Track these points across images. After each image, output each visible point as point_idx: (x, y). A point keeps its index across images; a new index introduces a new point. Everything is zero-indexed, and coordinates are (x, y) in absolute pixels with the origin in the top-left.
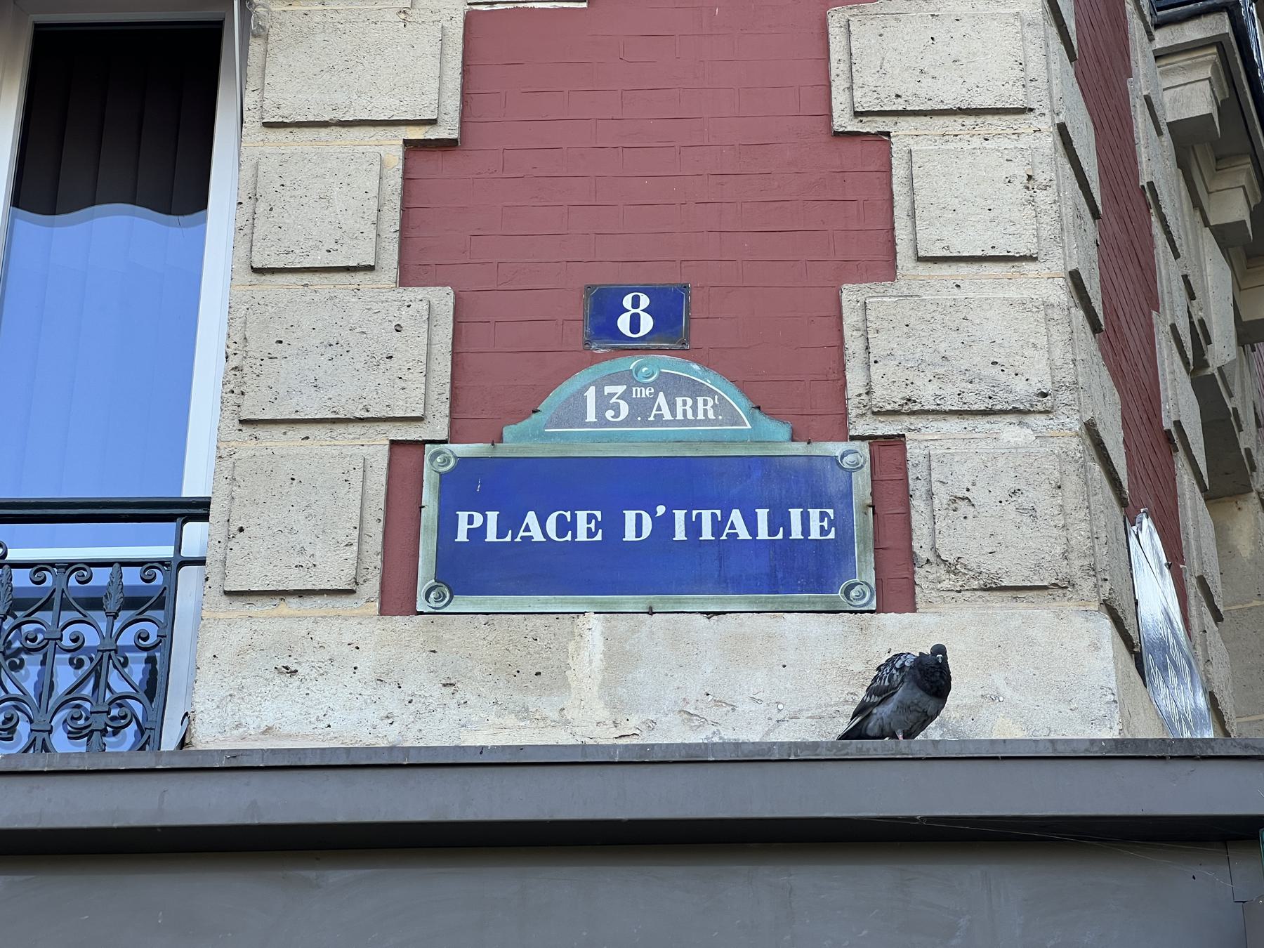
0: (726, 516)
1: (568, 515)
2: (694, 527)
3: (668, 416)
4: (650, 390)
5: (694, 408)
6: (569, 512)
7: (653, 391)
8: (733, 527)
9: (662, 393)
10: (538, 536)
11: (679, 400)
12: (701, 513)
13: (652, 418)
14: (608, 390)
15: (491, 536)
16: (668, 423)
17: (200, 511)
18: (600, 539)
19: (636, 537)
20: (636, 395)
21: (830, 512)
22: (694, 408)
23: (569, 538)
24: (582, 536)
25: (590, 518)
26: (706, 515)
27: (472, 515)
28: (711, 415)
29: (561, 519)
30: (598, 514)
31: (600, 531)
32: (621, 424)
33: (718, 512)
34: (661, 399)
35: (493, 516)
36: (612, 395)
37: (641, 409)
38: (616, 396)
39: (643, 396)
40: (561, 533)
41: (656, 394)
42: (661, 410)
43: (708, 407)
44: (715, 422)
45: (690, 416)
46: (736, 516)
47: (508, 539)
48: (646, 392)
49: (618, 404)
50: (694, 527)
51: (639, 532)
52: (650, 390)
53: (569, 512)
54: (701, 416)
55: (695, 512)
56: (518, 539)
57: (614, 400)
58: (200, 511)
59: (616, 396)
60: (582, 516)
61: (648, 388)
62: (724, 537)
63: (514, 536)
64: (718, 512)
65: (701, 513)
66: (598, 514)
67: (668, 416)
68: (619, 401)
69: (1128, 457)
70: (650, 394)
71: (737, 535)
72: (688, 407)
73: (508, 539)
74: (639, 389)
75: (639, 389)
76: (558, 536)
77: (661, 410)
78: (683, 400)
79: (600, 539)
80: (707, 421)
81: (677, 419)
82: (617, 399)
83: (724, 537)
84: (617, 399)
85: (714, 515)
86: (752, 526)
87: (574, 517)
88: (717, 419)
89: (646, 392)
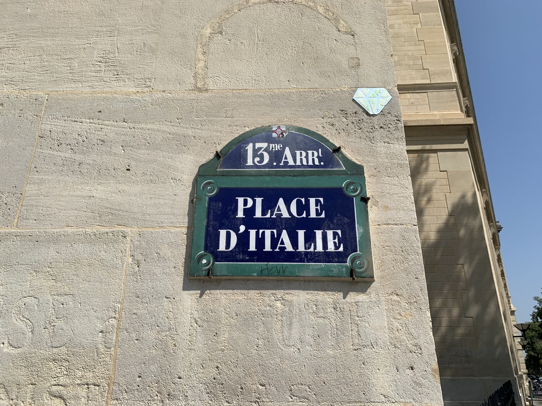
0: (279, 235)
2: (260, 242)
3: (291, 163)
4: (280, 146)
7: (281, 146)
8: (282, 243)
9: (252, 144)
10: (285, 215)
11: (298, 153)
13: (282, 164)
14: (258, 145)
15: (258, 214)
16: (291, 167)
18: (260, 230)
22: (307, 157)
23: (304, 215)
24: (313, 215)
26: (268, 233)
28: (317, 163)
31: (324, 211)
32: (265, 166)
33: (275, 231)
34: (287, 152)
36: (260, 149)
37: (277, 156)
38: (263, 149)
39: (277, 149)
40: (299, 212)
43: (315, 157)
44: (319, 166)
45: (305, 163)
46: (285, 235)
47: (268, 216)
48: (278, 147)
49: (262, 154)
50: (260, 242)
52: (280, 146)
55: (261, 231)
56: (274, 216)
57: (261, 152)
59: (263, 149)
62: (277, 250)
63: (272, 215)
64: (275, 231)
65: (265, 231)
67: (291, 163)
68: (262, 152)
69: (477, 172)
70: (280, 148)
71: (285, 248)
72: (303, 157)
73: (268, 216)
74: (274, 145)
76: (298, 215)
77: (287, 159)
78: (312, 152)
79: (260, 230)
80: (314, 166)
81: (308, 164)
82: (262, 151)
83: (277, 250)
84: (262, 151)
86: (294, 242)
87: (308, 202)
89: (278, 147)
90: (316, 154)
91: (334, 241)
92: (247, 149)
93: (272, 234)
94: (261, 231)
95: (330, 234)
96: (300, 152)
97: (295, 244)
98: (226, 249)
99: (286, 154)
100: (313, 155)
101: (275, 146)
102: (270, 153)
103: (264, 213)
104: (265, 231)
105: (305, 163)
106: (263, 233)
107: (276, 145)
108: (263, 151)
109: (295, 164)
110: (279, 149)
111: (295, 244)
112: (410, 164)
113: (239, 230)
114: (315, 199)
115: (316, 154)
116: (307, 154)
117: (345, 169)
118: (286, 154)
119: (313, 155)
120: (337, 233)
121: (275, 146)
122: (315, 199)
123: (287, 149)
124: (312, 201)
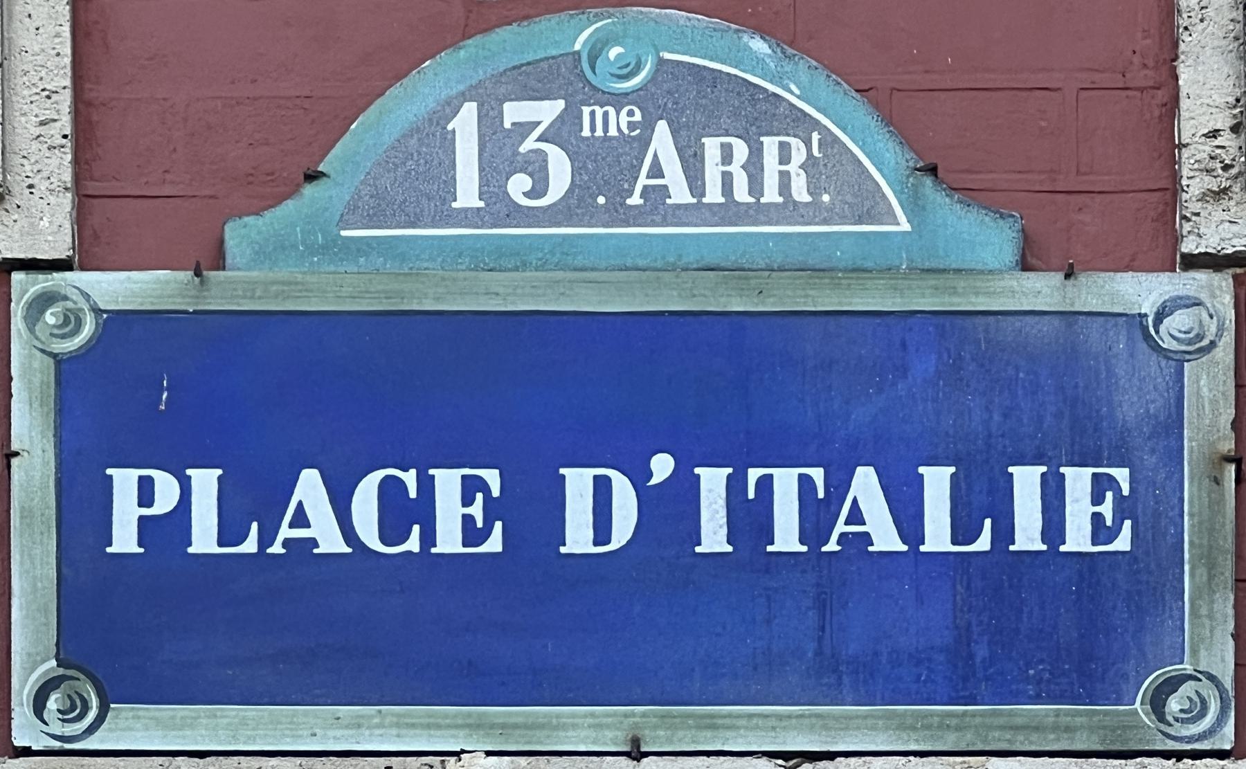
0: (839, 484)
3: (680, 194)
5: (754, 167)
7: (638, 116)
8: (856, 516)
11: (712, 146)
13: (635, 200)
14: (514, 112)
16: (679, 214)
21: (1121, 475)
22: (754, 167)
24: (449, 541)
26: (785, 481)
28: (800, 193)
33: (817, 474)
34: (662, 140)
35: (205, 481)
36: (524, 129)
39: (613, 132)
40: (392, 530)
41: (648, 127)
47: (250, 546)
48: (620, 121)
52: (631, 113)
55: (754, 474)
57: (529, 144)
62: (832, 546)
63: (266, 539)
64: (817, 474)
67: (680, 194)
70: (632, 126)
72: (736, 168)
73: (250, 546)
74: (599, 112)
75: (599, 112)
76: (384, 540)
80: (788, 210)
82: (538, 140)
83: (832, 546)
87: (426, 485)
89: (620, 121)
90: (799, 154)
91: (1097, 509)
92: (454, 131)
93: (805, 483)
94: (754, 474)
95: (1078, 480)
96: (722, 145)
97: (908, 522)
98: (596, 543)
99: (655, 155)
100: (785, 158)
101: (606, 114)
102: (580, 153)
103: (229, 532)
104: (771, 476)
105: (742, 194)
106: (765, 484)
107: (611, 110)
108: (540, 139)
109: (752, 200)
110: (626, 131)
111: (908, 522)
112: (88, 96)
113: (650, 475)
114: (464, 477)
115: (799, 154)
116: (756, 153)
117: (905, 226)
118: (655, 155)
119: (785, 158)
120: (1111, 478)
121: (606, 114)
122: (464, 477)
123: (662, 127)
124: (447, 481)
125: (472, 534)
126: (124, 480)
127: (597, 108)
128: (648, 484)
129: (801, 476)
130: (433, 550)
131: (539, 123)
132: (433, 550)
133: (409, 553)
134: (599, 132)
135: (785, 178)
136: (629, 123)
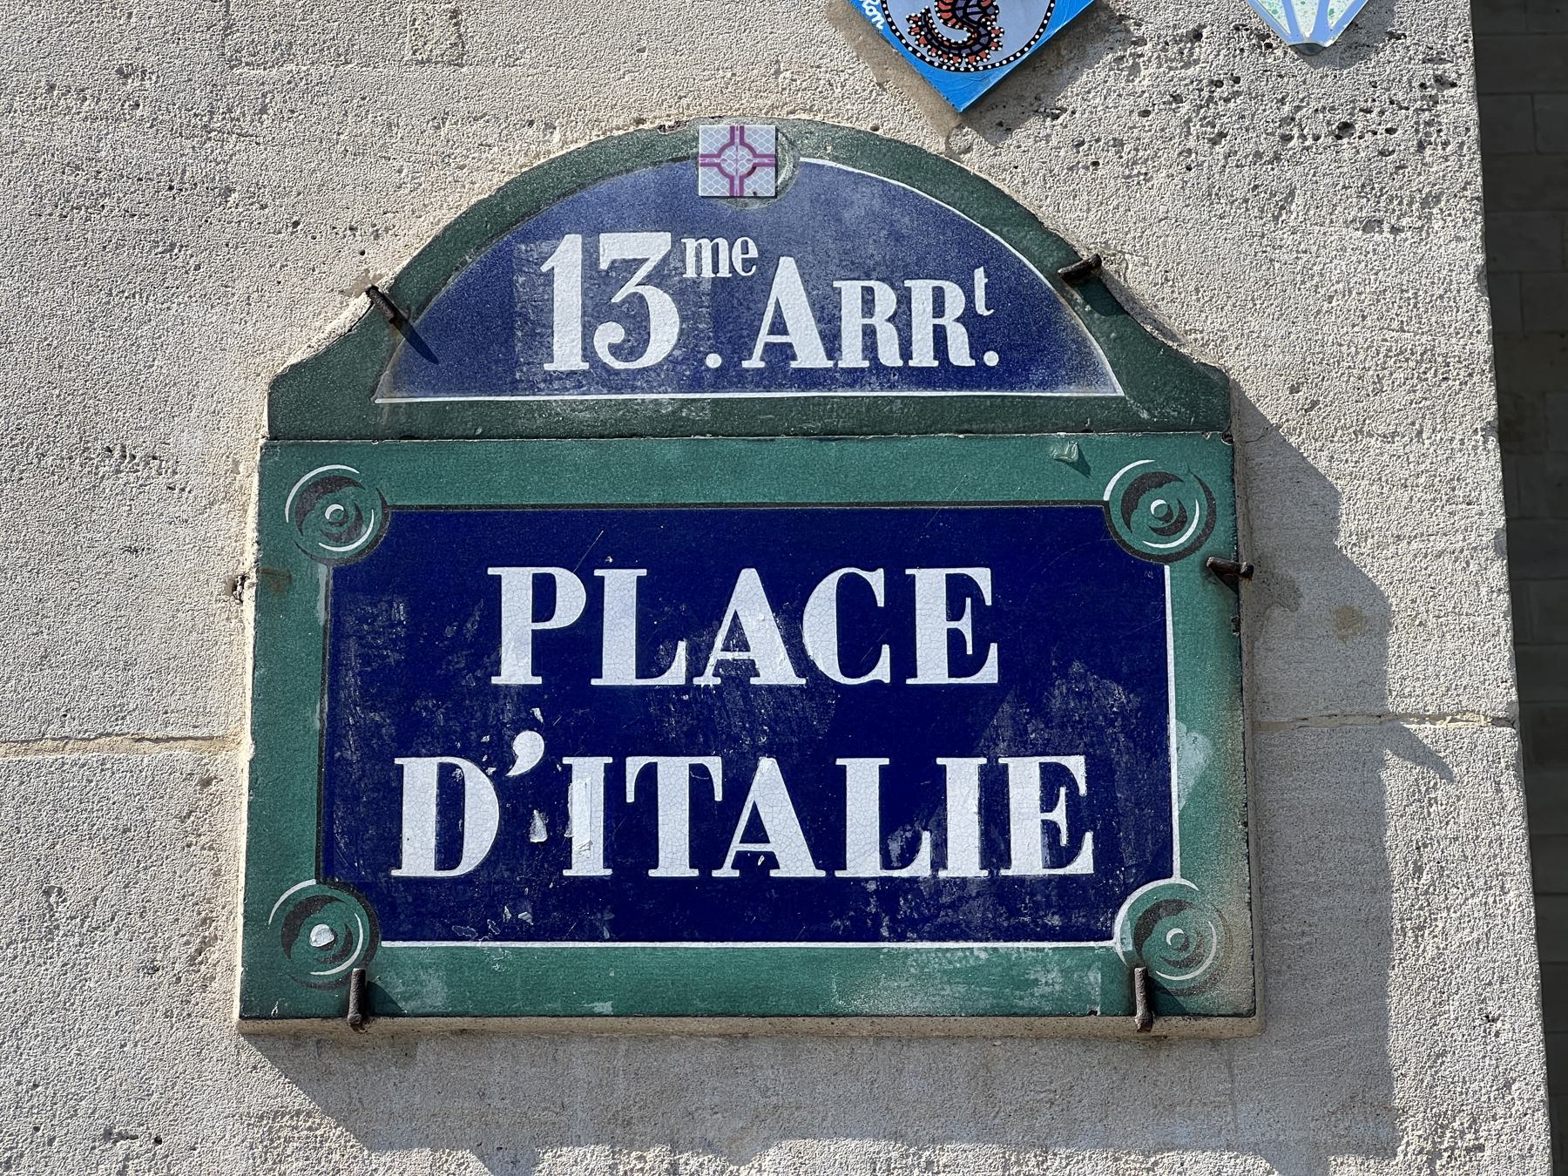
0: (739, 785)
1: (876, 580)
4: (745, 250)
5: (902, 319)
6: (881, 571)
7: (753, 252)
11: (850, 291)
12: (656, 764)
13: (755, 362)
14: (614, 246)
16: (809, 378)
17: (737, 133)
19: (439, 867)
20: (716, 269)
21: (1076, 765)
22: (902, 319)
23: (882, 672)
24: (932, 668)
25: (959, 591)
26: (674, 774)
27: (551, 579)
28: (960, 355)
29: (852, 597)
30: (982, 577)
31: (994, 648)
33: (714, 764)
35: (621, 585)
39: (724, 272)
40: (854, 655)
41: (765, 267)
42: (785, 332)
43: (948, 321)
45: (889, 355)
51: (450, 845)
52: (745, 250)
53: (881, 571)
54: (923, 357)
55: (634, 765)
58: (737, 133)
60: (930, 584)
61: (739, 241)
63: (695, 669)
64: (714, 764)
65: (656, 764)
66: (982, 577)
68: (640, 289)
70: (747, 264)
73: (675, 675)
76: (845, 671)
77: (785, 332)
85: (699, 779)
87: (902, 592)
88: (981, 364)
94: (634, 765)
95: (1024, 775)
101: (715, 251)
105: (889, 355)
106: (648, 777)
107: (723, 243)
116: (904, 299)
117: (1120, 392)
119: (939, 310)
120: (1064, 771)
125: (960, 662)
126: (516, 584)
127: (705, 242)
128: (511, 773)
129: (693, 768)
130: (610, 760)
131: (646, 260)
132: (610, 760)
133: (877, 684)
134: (707, 273)
135: (940, 335)
136: (744, 260)
